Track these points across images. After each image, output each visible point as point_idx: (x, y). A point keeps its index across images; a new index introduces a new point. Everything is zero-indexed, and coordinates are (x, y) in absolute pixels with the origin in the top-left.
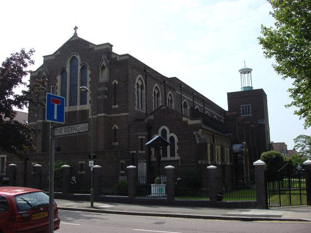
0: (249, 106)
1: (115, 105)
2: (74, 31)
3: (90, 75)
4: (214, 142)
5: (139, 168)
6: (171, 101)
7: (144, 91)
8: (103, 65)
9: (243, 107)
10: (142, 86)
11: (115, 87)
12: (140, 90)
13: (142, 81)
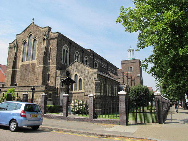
2: (32, 21)
3: (38, 44)
4: (106, 83)
6: (87, 61)
7: (68, 54)
12: (86, 62)
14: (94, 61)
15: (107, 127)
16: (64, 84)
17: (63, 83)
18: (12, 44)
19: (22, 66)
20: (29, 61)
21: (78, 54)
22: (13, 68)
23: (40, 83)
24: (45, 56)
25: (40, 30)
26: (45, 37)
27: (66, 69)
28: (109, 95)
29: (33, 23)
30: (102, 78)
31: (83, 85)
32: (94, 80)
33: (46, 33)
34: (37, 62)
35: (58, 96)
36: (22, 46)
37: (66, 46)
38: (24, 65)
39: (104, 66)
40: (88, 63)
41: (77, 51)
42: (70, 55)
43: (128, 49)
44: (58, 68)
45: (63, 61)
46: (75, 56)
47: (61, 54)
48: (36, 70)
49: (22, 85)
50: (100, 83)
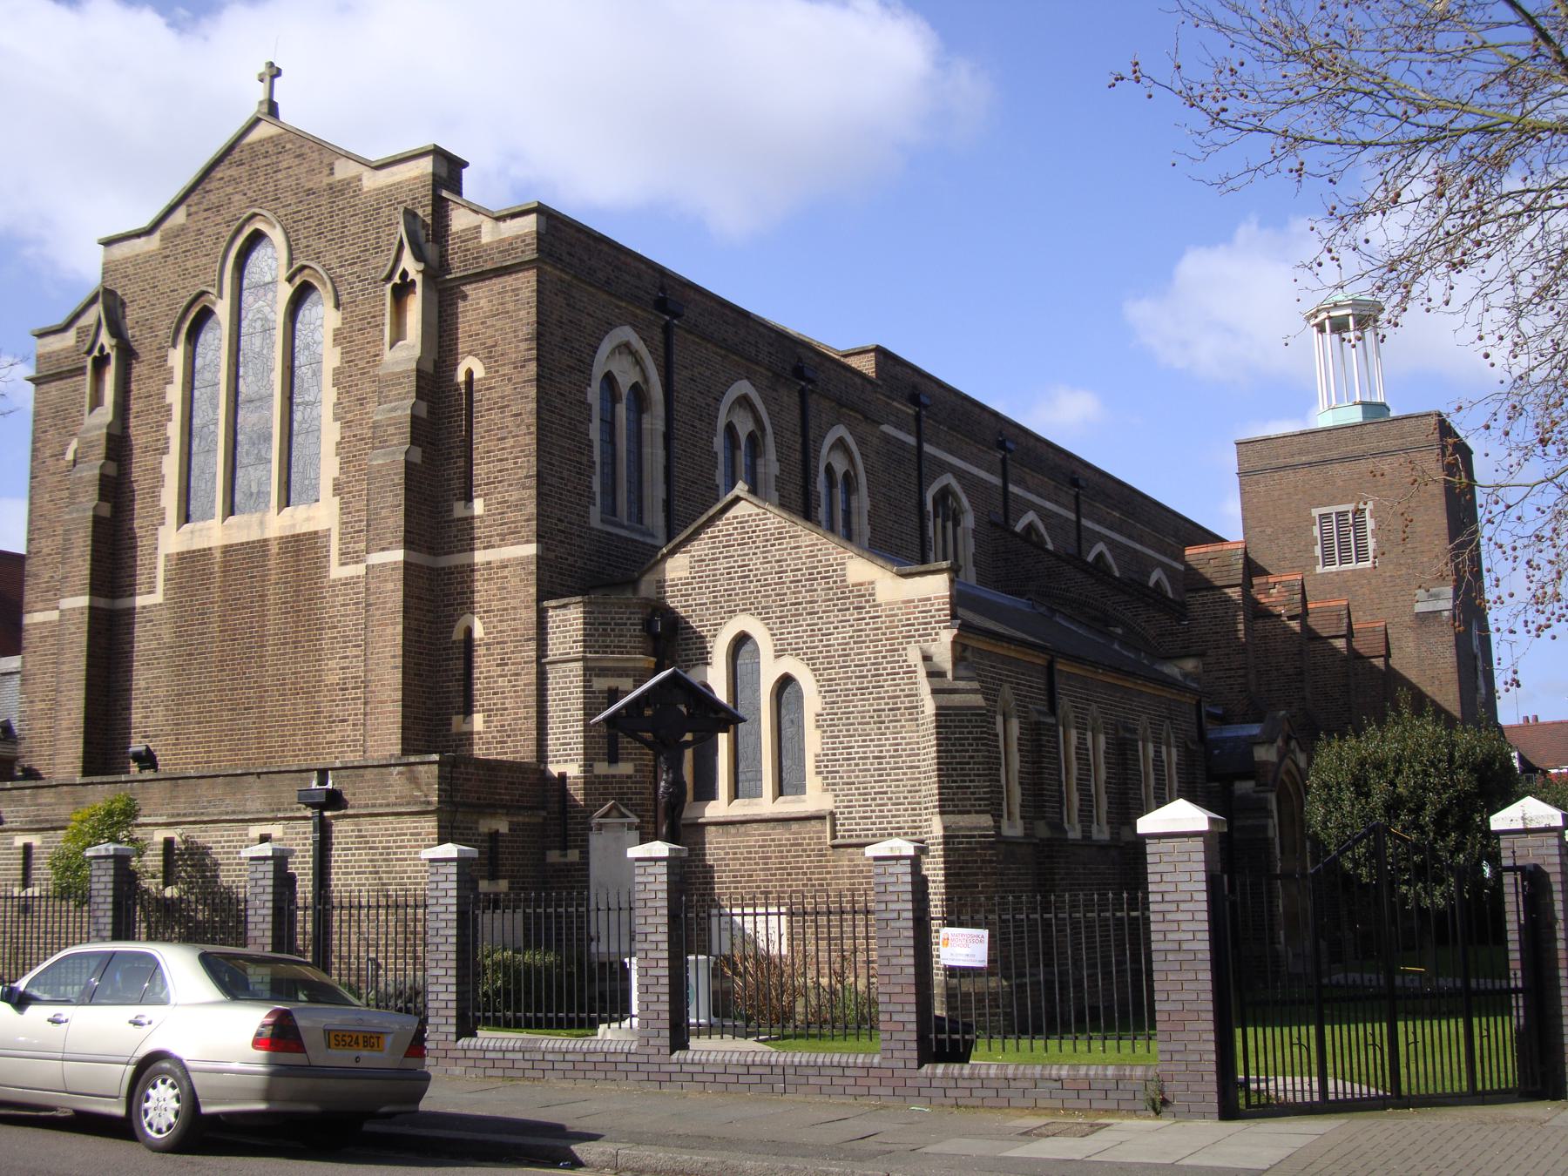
0: (1359, 512)
3: (337, 372)
4: (1052, 710)
6: (849, 481)
7: (654, 422)
8: (404, 274)
9: (1361, 555)
10: (639, 395)
12: (839, 494)
13: (638, 362)
14: (923, 469)
15: (1043, 1130)
16: (624, 741)
17: (606, 739)
18: (71, 334)
19: (190, 563)
20: (256, 517)
21: (758, 420)
22: (95, 589)
23: (387, 737)
24: (417, 456)
25: (346, 184)
26: (409, 264)
27: (634, 584)
28: (1086, 832)
29: (272, 109)
30: (1005, 660)
31: (813, 742)
32: (924, 687)
33: (410, 215)
34: (329, 509)
35: (574, 855)
36: (177, 357)
37: (626, 348)
38: (206, 553)
39: (1043, 514)
40: (862, 501)
42: (668, 437)
44: (553, 582)
45: (610, 509)
46: (719, 442)
48: (336, 608)
49: (202, 757)
50: (982, 718)
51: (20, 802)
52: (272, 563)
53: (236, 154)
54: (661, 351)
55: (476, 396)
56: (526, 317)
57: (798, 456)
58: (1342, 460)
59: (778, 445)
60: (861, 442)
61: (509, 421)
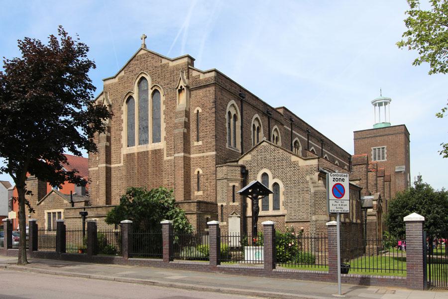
0: (375, 159)
1: (198, 141)
3: (164, 111)
5: (230, 224)
7: (239, 123)
8: (181, 87)
10: (235, 116)
11: (197, 116)
12: (232, 120)
13: (236, 109)
14: (292, 136)
19: (129, 156)
21: (259, 124)
27: (237, 161)
29: (145, 46)
35: (225, 223)
39: (315, 147)
41: (257, 116)
42: (242, 127)
43: (373, 99)
45: (230, 144)
47: (223, 124)
48: (166, 166)
51: (93, 211)
52: (150, 156)
53: (136, 58)
54: (240, 106)
55: (199, 117)
56: (212, 97)
57: (268, 132)
58: (380, 136)
59: (264, 130)
60: (280, 129)
61: (208, 123)
